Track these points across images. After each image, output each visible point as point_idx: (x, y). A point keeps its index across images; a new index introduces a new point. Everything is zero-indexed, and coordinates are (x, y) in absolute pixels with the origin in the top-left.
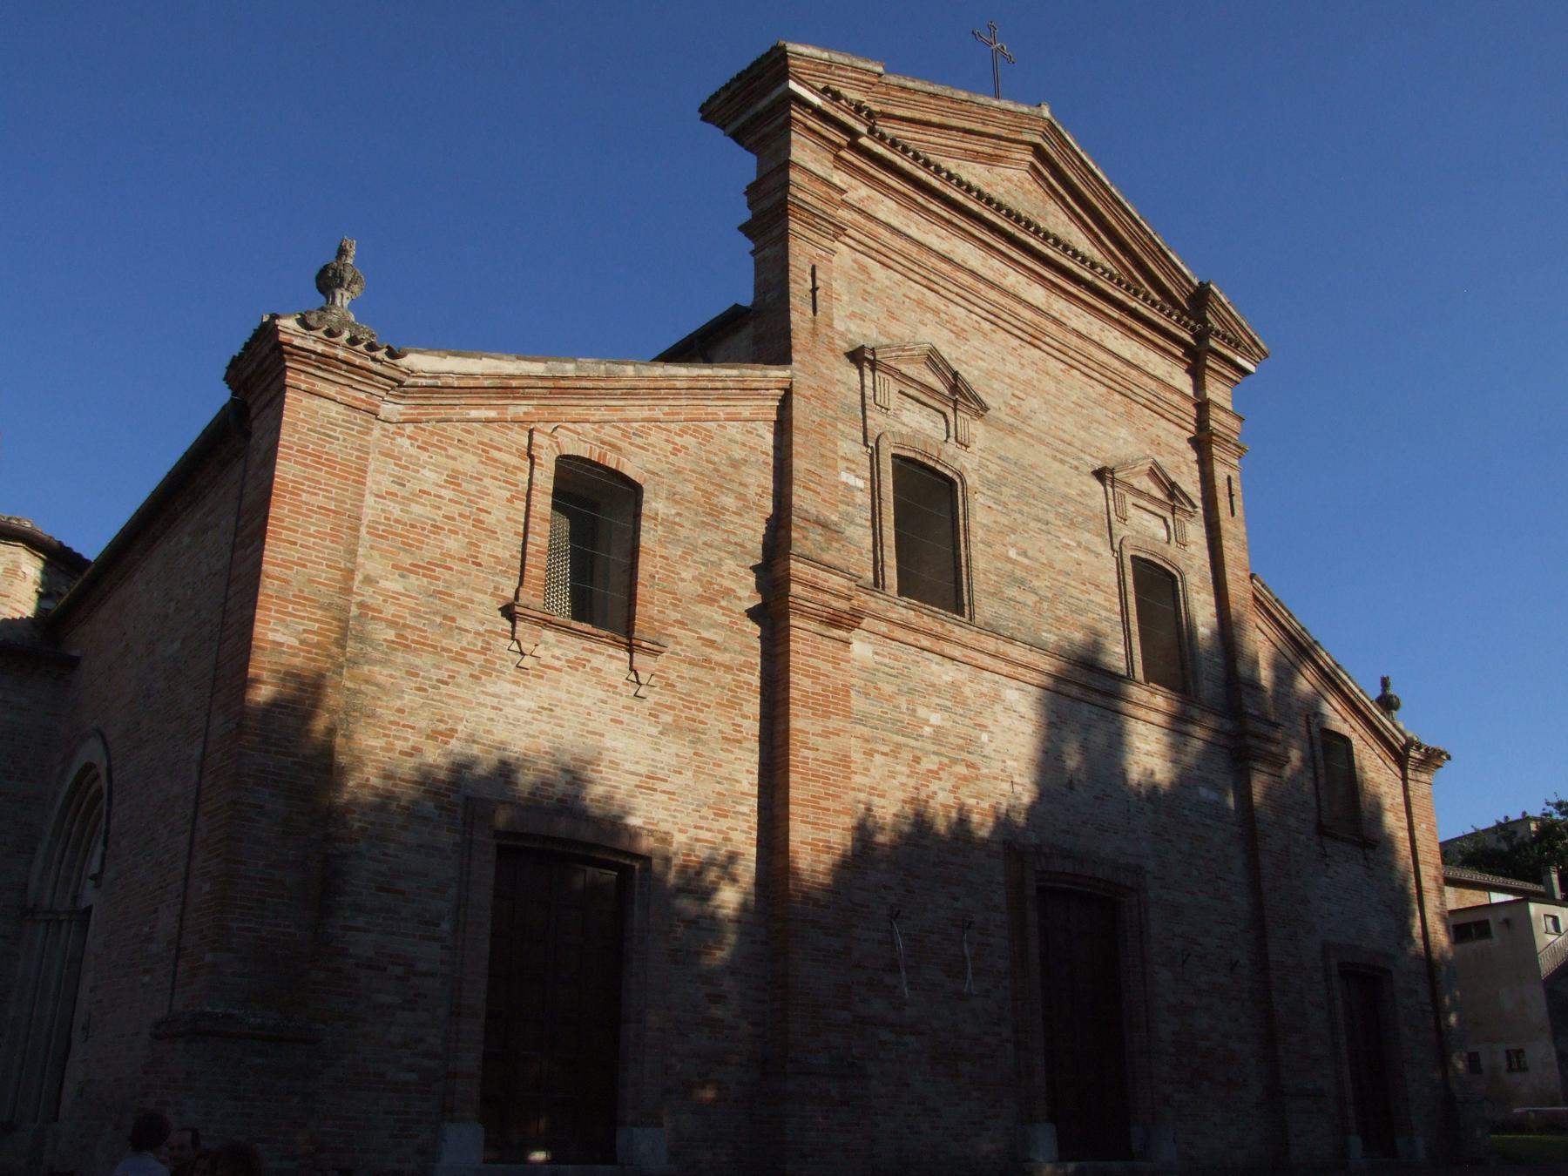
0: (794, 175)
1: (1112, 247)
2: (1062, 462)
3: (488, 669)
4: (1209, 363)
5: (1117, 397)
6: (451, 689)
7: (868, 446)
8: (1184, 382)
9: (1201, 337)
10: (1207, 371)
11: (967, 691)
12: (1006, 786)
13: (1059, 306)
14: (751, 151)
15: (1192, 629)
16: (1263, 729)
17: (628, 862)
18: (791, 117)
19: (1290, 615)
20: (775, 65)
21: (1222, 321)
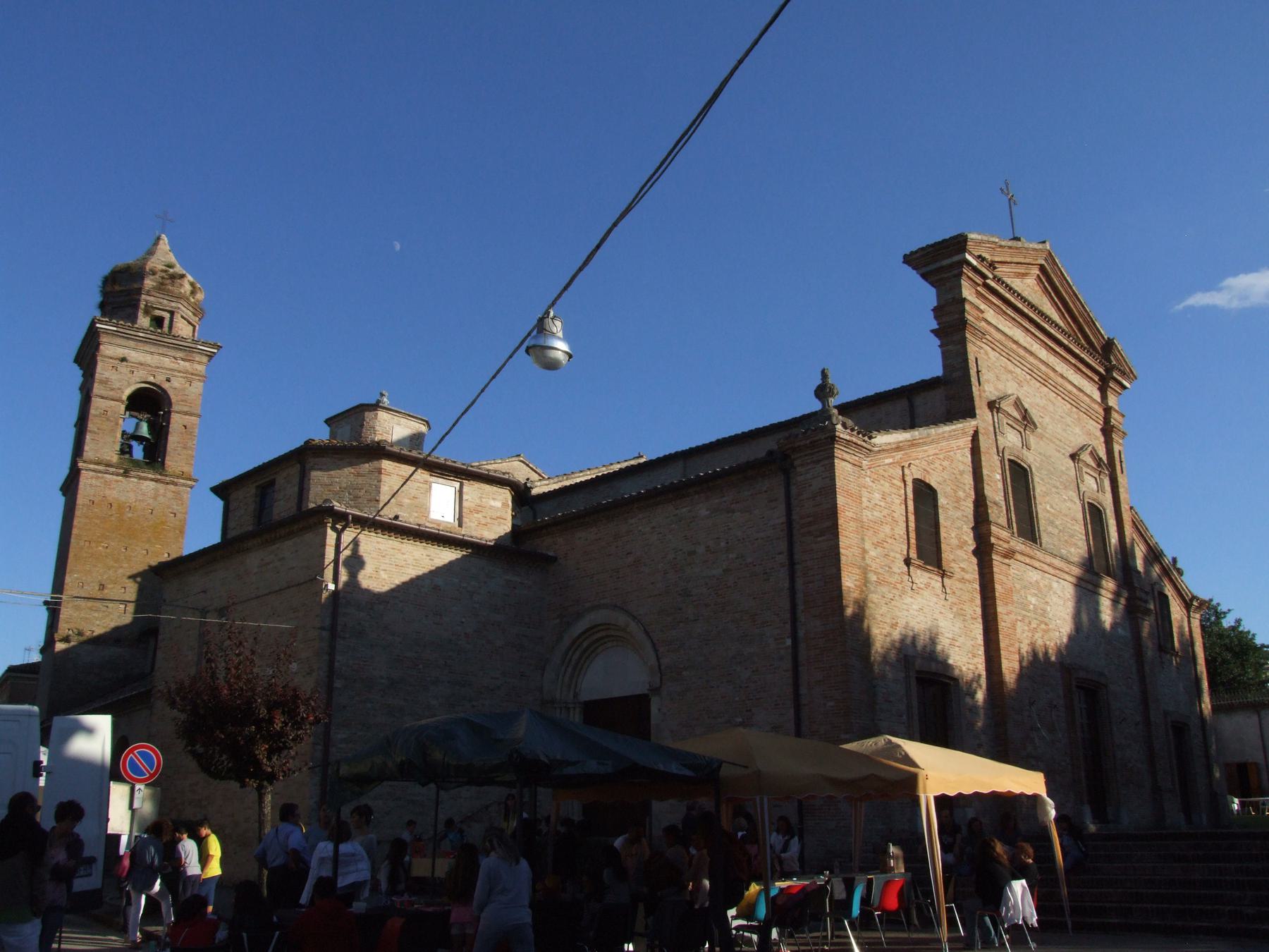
0: (967, 307)
1: (1069, 320)
2: (1059, 451)
3: (904, 592)
4: (1111, 385)
5: (1075, 409)
6: (893, 603)
7: (999, 456)
8: (1097, 395)
9: (1109, 370)
10: (1109, 389)
11: (1041, 585)
12: (1058, 633)
13: (1052, 360)
14: (933, 285)
15: (1126, 543)
16: (1143, 595)
17: (947, 681)
18: (962, 271)
19: (1147, 529)
20: (959, 243)
21: (1117, 360)
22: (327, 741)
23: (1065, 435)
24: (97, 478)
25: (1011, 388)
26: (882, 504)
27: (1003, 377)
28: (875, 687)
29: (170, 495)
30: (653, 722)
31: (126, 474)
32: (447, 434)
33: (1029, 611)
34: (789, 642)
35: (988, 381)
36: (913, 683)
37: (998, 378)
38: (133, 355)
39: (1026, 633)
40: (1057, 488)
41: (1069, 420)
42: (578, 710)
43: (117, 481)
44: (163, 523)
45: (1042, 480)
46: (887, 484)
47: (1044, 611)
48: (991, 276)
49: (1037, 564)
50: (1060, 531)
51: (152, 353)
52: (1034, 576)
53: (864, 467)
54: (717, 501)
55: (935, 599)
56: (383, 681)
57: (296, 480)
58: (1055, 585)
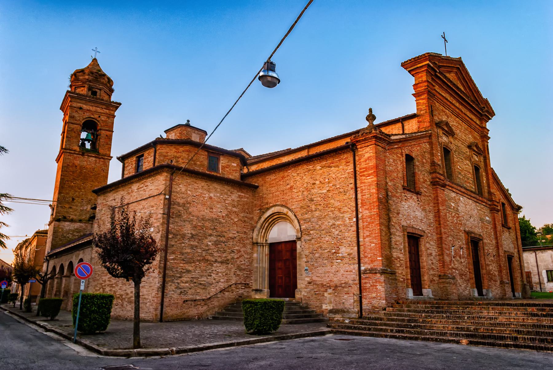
22: (166, 260)
23: (465, 138)
24: (71, 156)
25: (444, 119)
26: (393, 164)
27: (441, 114)
28: (391, 238)
29: (101, 163)
30: (298, 251)
31: (83, 155)
32: (218, 126)
33: (451, 209)
34: (355, 220)
35: (435, 115)
36: (406, 237)
37: (439, 114)
38: (85, 107)
39: (450, 218)
40: (462, 159)
41: (467, 132)
42: (267, 246)
43: (78, 157)
44: (99, 174)
45: (456, 156)
46: (395, 156)
47: (457, 209)
48: (438, 71)
49: (454, 190)
50: (463, 177)
51: (92, 106)
52: (453, 195)
53: (387, 149)
54: (324, 163)
55: (415, 204)
56: (189, 235)
57: (153, 154)
58: (461, 199)
